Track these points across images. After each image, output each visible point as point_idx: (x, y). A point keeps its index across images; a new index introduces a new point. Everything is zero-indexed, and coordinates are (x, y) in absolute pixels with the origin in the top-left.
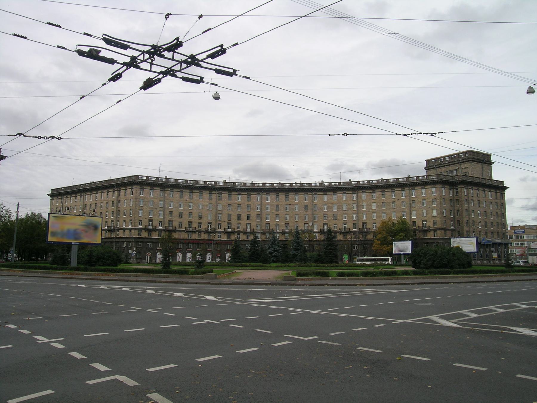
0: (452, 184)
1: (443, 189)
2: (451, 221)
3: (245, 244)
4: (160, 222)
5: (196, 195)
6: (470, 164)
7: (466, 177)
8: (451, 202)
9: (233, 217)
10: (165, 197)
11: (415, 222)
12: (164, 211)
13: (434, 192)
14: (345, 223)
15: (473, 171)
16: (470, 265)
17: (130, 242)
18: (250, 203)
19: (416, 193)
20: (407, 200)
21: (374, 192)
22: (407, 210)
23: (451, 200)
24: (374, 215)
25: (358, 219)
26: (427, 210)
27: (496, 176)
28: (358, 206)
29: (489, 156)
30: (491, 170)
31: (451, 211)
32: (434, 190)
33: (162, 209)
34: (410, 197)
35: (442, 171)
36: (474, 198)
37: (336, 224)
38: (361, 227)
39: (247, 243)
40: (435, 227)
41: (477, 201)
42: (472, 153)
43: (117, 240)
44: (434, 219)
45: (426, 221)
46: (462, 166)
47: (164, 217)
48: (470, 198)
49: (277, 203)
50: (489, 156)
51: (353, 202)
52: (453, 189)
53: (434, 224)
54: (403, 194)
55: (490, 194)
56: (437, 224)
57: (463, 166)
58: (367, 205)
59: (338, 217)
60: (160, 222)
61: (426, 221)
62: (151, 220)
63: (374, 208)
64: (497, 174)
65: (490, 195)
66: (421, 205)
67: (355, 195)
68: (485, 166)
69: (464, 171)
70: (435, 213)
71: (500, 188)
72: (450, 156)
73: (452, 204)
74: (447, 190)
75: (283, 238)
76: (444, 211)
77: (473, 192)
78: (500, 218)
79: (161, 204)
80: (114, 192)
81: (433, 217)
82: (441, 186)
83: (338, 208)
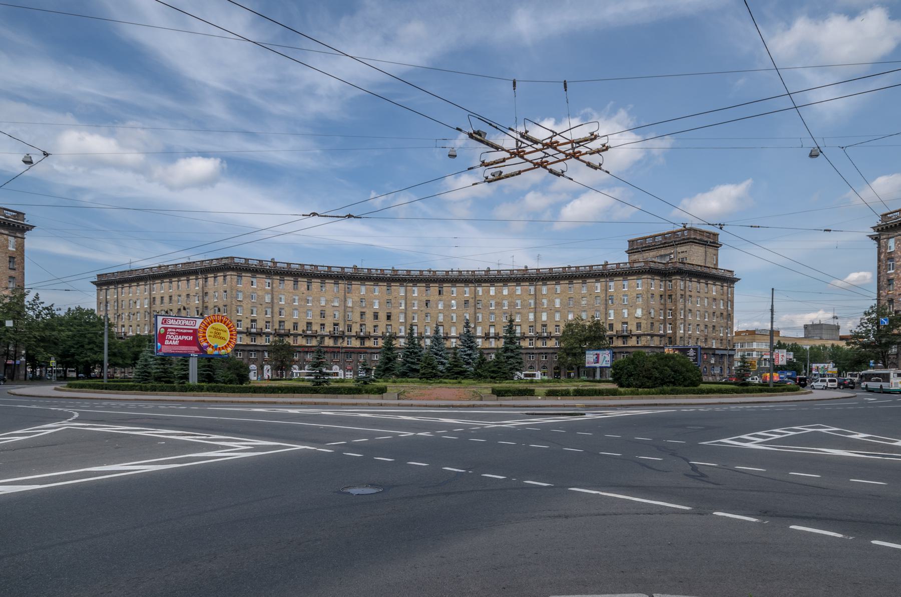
10: (272, 288)
12: (272, 308)
13: (639, 285)
15: (695, 256)
22: (602, 308)
28: (535, 303)
32: (640, 282)
36: (692, 294)
40: (639, 332)
44: (638, 321)
45: (626, 323)
48: (688, 293)
53: (639, 326)
55: (714, 288)
58: (549, 301)
61: (626, 323)
62: (253, 321)
63: (558, 305)
64: (726, 260)
65: (714, 290)
67: (532, 288)
68: (711, 250)
70: (639, 313)
71: (728, 280)
77: (694, 285)
79: (268, 299)
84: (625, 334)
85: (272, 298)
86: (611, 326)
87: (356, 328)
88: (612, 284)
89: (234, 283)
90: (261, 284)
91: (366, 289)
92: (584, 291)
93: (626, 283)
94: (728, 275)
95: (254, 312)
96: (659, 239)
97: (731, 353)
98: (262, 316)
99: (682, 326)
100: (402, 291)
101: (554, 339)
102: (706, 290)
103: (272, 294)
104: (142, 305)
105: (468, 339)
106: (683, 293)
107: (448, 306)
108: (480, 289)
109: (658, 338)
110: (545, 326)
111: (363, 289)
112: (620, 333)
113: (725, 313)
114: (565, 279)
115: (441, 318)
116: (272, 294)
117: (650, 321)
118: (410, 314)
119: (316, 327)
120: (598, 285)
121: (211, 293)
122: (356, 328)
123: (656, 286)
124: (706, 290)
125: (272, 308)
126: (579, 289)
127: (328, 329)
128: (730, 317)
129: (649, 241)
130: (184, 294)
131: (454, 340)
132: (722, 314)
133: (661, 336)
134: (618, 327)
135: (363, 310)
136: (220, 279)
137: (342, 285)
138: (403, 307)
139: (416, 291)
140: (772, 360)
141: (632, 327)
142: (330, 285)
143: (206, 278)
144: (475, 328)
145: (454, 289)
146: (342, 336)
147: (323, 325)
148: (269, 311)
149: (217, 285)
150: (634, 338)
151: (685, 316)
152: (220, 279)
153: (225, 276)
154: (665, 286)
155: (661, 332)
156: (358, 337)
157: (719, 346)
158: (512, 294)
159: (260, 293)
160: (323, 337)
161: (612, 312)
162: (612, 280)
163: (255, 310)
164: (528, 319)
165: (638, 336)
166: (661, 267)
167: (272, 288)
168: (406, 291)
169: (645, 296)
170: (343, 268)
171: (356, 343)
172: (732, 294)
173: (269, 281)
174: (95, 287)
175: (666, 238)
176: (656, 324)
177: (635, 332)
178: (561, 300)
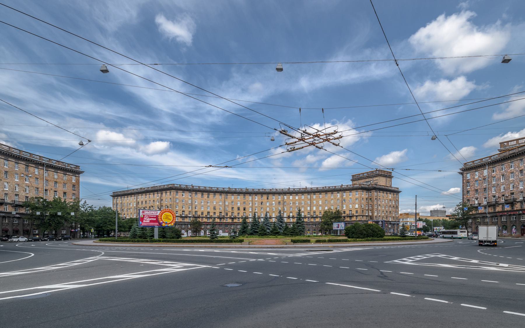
9: (235, 209)
15: (382, 182)
20: (341, 199)
21: (321, 194)
22: (340, 204)
30: (391, 181)
40: (357, 214)
55: (390, 195)
57: (375, 179)
62: (183, 211)
65: (390, 196)
67: (309, 196)
68: (388, 179)
70: (357, 206)
71: (396, 192)
77: (381, 194)
79: (190, 202)
86: (344, 212)
87: (229, 214)
88: (345, 194)
89: (175, 195)
90: (187, 195)
98: (187, 209)
104: (133, 205)
107: (271, 204)
115: (268, 209)
118: (254, 208)
119: (211, 214)
120: (339, 194)
121: (164, 200)
122: (229, 214)
127: (217, 214)
128: (397, 207)
133: (367, 216)
136: (168, 193)
137: (223, 196)
139: (257, 198)
142: (218, 196)
144: (283, 213)
146: (223, 218)
147: (215, 213)
150: (355, 217)
152: (168, 193)
156: (230, 218)
158: (299, 199)
159: (186, 199)
160: (215, 218)
162: (344, 192)
165: (357, 216)
171: (230, 221)
172: (398, 198)
176: (365, 211)
177: (355, 214)
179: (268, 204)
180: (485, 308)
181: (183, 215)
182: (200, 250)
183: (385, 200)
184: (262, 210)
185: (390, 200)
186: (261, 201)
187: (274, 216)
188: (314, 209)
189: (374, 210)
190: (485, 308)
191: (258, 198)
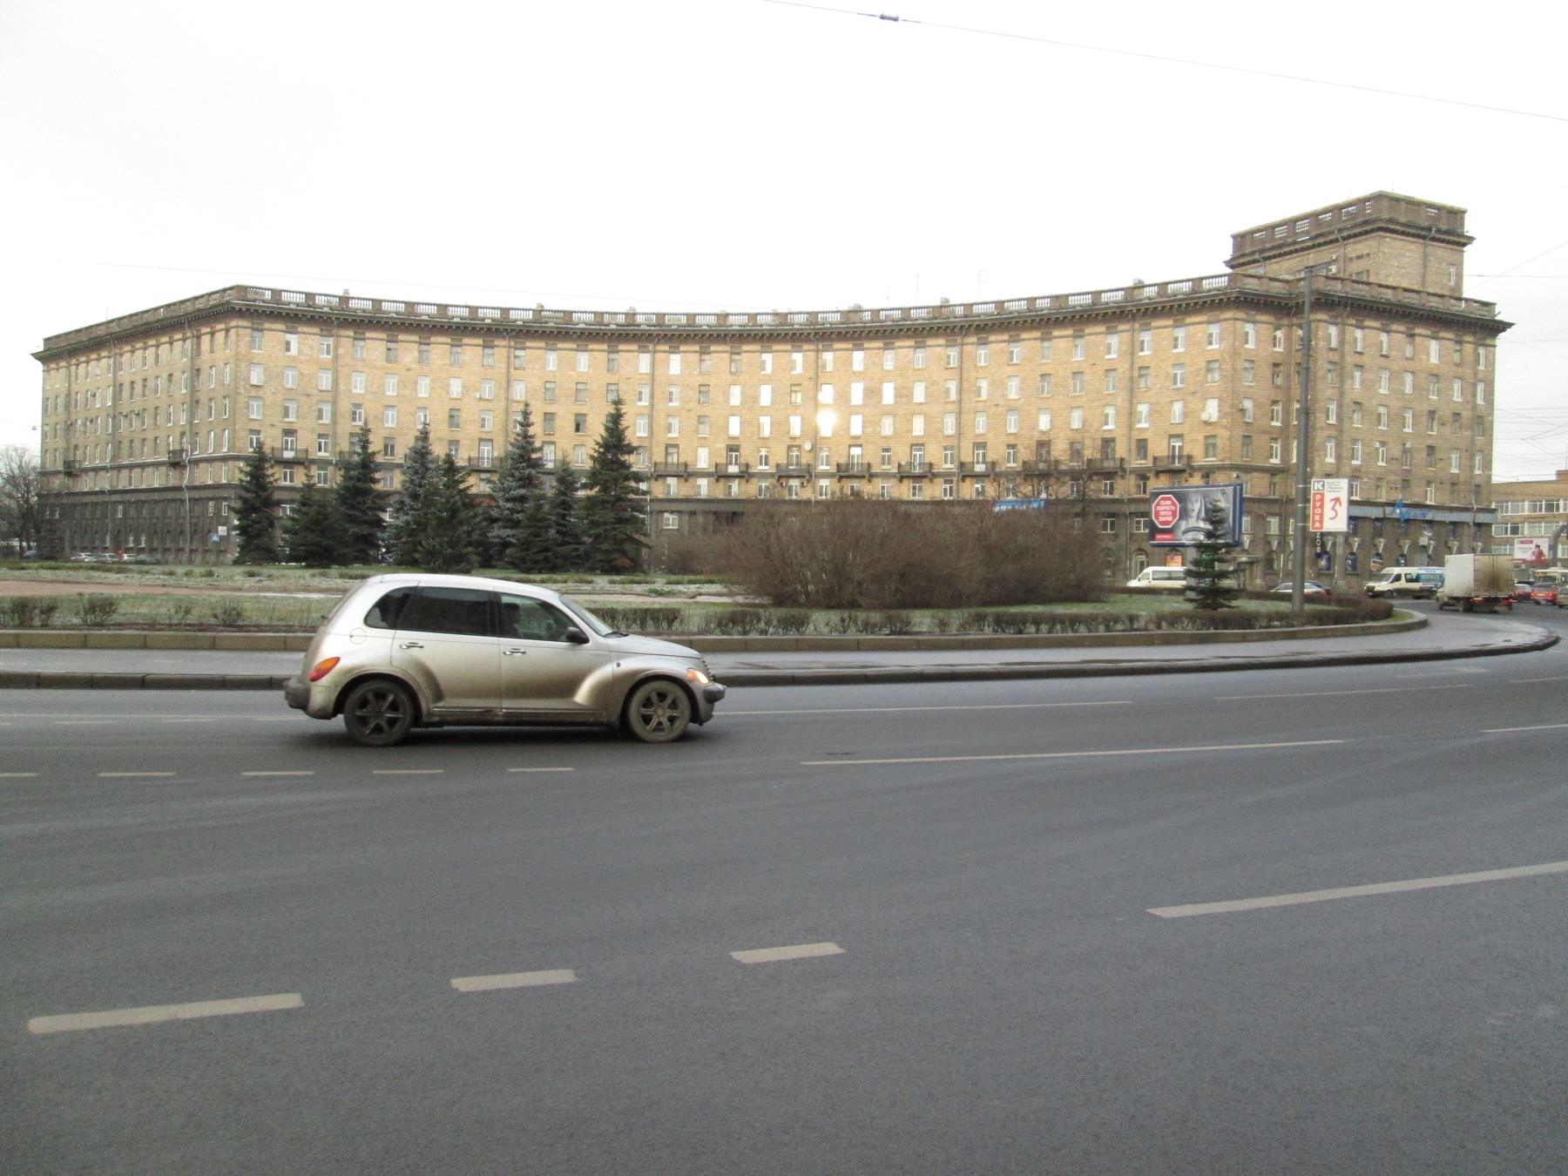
0: (1280, 307)
1: (1249, 328)
2: (1275, 440)
3: (662, 512)
4: (320, 436)
5: (440, 347)
6: (1373, 243)
7: (1357, 280)
8: (1274, 375)
9: (559, 422)
10: (336, 357)
11: (1145, 440)
12: (334, 403)
13: (1209, 336)
14: (918, 445)
15: (1395, 265)
16: (1388, 613)
17: (225, 499)
18: (614, 379)
19: (1154, 340)
20: (1123, 367)
21: (1015, 340)
22: (1121, 399)
23: (1276, 365)
24: (1012, 419)
25: (959, 434)
26: (1183, 400)
27: (1472, 289)
28: (960, 391)
29: (1456, 215)
30: (1459, 265)
31: (1275, 402)
32: (1215, 329)
33: (329, 397)
34: (1133, 354)
35: (1285, 269)
36: (1365, 360)
37: (887, 450)
38: (966, 458)
39: (667, 506)
40: (1212, 461)
41: (1383, 372)
42: (1385, 203)
43: (196, 494)
44: (1208, 431)
45: (1180, 436)
46: (1349, 248)
47: (334, 423)
48: (1350, 359)
49: (701, 380)
50: (1456, 215)
51: (946, 374)
52: (1290, 326)
53: (1209, 447)
54: (1112, 344)
55: (1434, 346)
56: (1219, 449)
57: (1354, 249)
58: (993, 384)
59: (1439, 455)
60: (320, 436)
61: (1180, 436)
62: (289, 432)
63: (1013, 395)
64: (1480, 277)
65: (1435, 350)
66: (1169, 383)
67: (953, 353)
68: (1439, 252)
69: (1355, 267)
70: (1212, 410)
71: (1483, 326)
72: (1313, 216)
73: (1279, 381)
74: (1266, 330)
75: (719, 492)
76: (1248, 404)
77: (1366, 337)
78: (1467, 433)
79: (325, 381)
80: (212, 334)
81: (1206, 423)
82: (1240, 315)
83: (898, 395)
84: (1177, 465)
85: (336, 381)
86: (1142, 445)
88: (1146, 337)
89: (243, 348)
90: (304, 344)
91: (560, 361)
92: (1078, 357)
93: (1180, 333)
94: (1479, 313)
95: (292, 412)
96: (1303, 226)
97: (1482, 518)
98: (310, 422)
99: (1331, 446)
100: (644, 362)
101: (940, 480)
102: (1409, 351)
103: (336, 372)
104: (103, 401)
105: (523, 458)
106: (1335, 357)
107: (751, 399)
108: (828, 357)
109: (1266, 478)
110: (983, 445)
111: (552, 358)
112: (1162, 465)
113: (1466, 414)
114: (1032, 328)
115: (734, 428)
116: (336, 372)
117: (1240, 432)
118: (660, 419)
120: (1114, 340)
121: (205, 368)
123: (1257, 336)
124: (1409, 351)
125: (334, 403)
126: (1065, 350)
128: (1481, 423)
129: (1280, 233)
130: (165, 376)
131: (824, 482)
132: (1457, 415)
133: (1273, 471)
134: (1158, 448)
135: (551, 409)
137: (501, 349)
138: (645, 403)
139: (675, 363)
140: (484, 534)
141: (1195, 450)
142: (471, 351)
143: (199, 337)
145: (767, 357)
148: (327, 409)
149: (222, 347)
151: (1340, 418)
153: (227, 331)
154: (1288, 339)
155: (1275, 461)
157: (1446, 500)
158: (901, 370)
159: (306, 369)
161: (1143, 409)
163: (292, 406)
164: (941, 430)
166: (1276, 288)
167: (336, 357)
168: (653, 363)
169: (1227, 367)
170: (505, 311)
172: (1491, 363)
173: (331, 341)
174: (39, 365)
175: (1320, 224)
176: (1260, 441)
177: (1200, 460)
178: (1023, 381)
179: (736, 396)
180: (39, 1025)
181: (288, 455)
182: (1013, 610)
183: (1395, 377)
184: (705, 430)
185: (1436, 376)
186: (697, 380)
187: (823, 468)
188: (918, 427)
189: (1320, 436)
190: (39, 1025)
191: (684, 363)
